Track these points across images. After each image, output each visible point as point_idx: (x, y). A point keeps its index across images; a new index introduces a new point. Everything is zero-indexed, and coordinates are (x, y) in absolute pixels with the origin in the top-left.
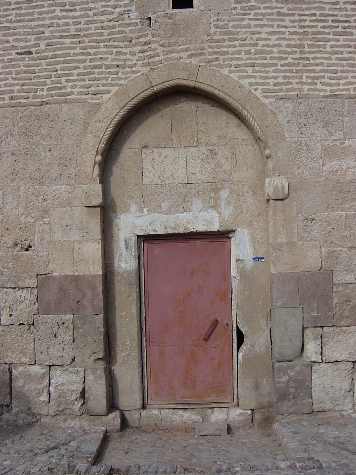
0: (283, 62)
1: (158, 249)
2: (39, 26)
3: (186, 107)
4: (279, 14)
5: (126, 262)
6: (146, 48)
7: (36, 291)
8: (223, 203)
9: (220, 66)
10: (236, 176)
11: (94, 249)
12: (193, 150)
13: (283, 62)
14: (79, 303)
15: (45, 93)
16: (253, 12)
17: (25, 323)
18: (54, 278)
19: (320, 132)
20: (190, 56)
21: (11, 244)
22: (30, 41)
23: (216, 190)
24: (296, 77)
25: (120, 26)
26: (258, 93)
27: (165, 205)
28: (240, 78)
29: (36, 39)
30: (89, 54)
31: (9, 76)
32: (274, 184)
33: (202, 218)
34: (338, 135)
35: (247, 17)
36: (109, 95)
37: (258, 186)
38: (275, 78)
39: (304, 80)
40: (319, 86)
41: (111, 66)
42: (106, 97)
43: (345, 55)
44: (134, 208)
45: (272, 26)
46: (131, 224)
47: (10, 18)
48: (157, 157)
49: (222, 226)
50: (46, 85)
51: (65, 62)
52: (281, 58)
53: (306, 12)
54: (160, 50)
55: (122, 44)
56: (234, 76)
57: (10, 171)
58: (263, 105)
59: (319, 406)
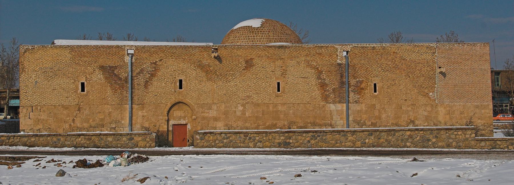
1: (176, 127)
3: (181, 104)
5: (171, 129)
11: (166, 126)
14: (299, 179)
19: (201, 109)
32: (194, 117)
33: (183, 122)
37: (191, 117)
46: (172, 122)
59: (321, 123)
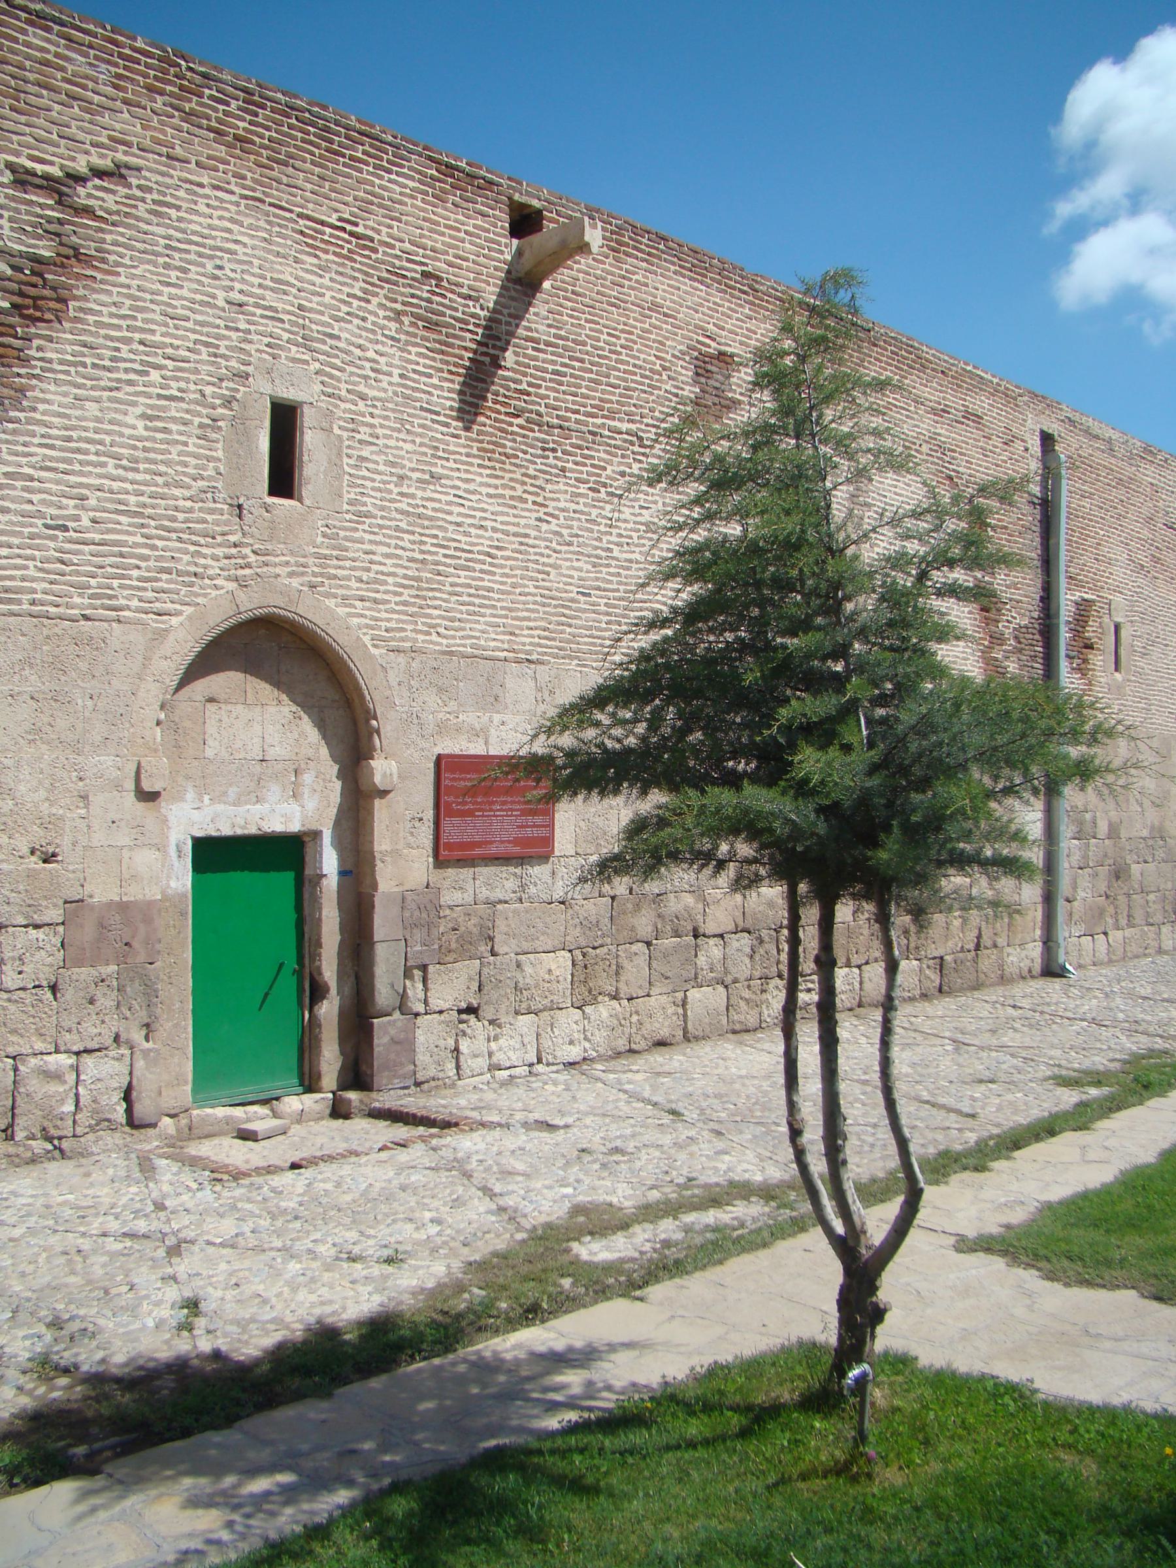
0: (398, 599)
2: (81, 485)
4: (398, 529)
6: (234, 551)
7: (61, 929)
8: (306, 791)
9: (328, 595)
13: (398, 599)
15: (86, 601)
16: (368, 521)
17: (45, 983)
18: (92, 908)
20: (291, 574)
21: (25, 850)
22: (66, 508)
24: (411, 622)
25: (201, 510)
26: (366, 640)
27: (233, 792)
28: (350, 615)
29: (76, 507)
30: (154, 548)
31: (31, 564)
35: (360, 527)
36: (181, 619)
38: (389, 620)
39: (420, 627)
40: (434, 637)
41: (188, 574)
42: (175, 621)
43: (466, 599)
44: (190, 795)
45: (389, 546)
47: (34, 459)
48: (225, 719)
50: (89, 587)
51: (122, 555)
52: (396, 594)
53: (427, 532)
54: (252, 558)
55: (202, 541)
56: (342, 611)
57: (27, 726)
58: (372, 657)
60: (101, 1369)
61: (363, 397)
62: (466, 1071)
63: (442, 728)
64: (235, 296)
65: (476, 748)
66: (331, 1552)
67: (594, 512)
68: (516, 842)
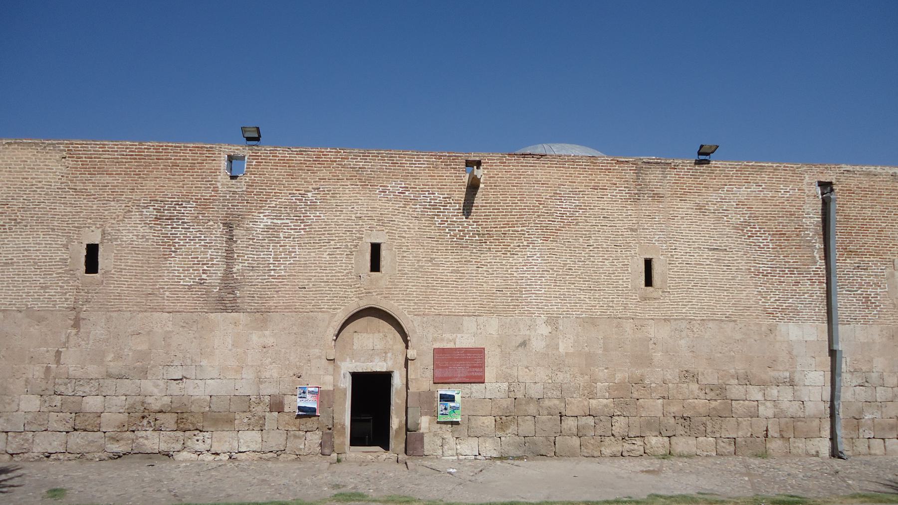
10: (395, 347)
12: (376, 334)
23: (386, 353)
34: (440, 332)
44: (348, 359)
49: (209, 150)
56: (396, 304)
60: (354, 491)
61: (404, 237)
62: (446, 453)
63: (435, 340)
64: (358, 215)
65: (451, 345)
66: (807, 176)
67: (504, 262)
68: (467, 377)
